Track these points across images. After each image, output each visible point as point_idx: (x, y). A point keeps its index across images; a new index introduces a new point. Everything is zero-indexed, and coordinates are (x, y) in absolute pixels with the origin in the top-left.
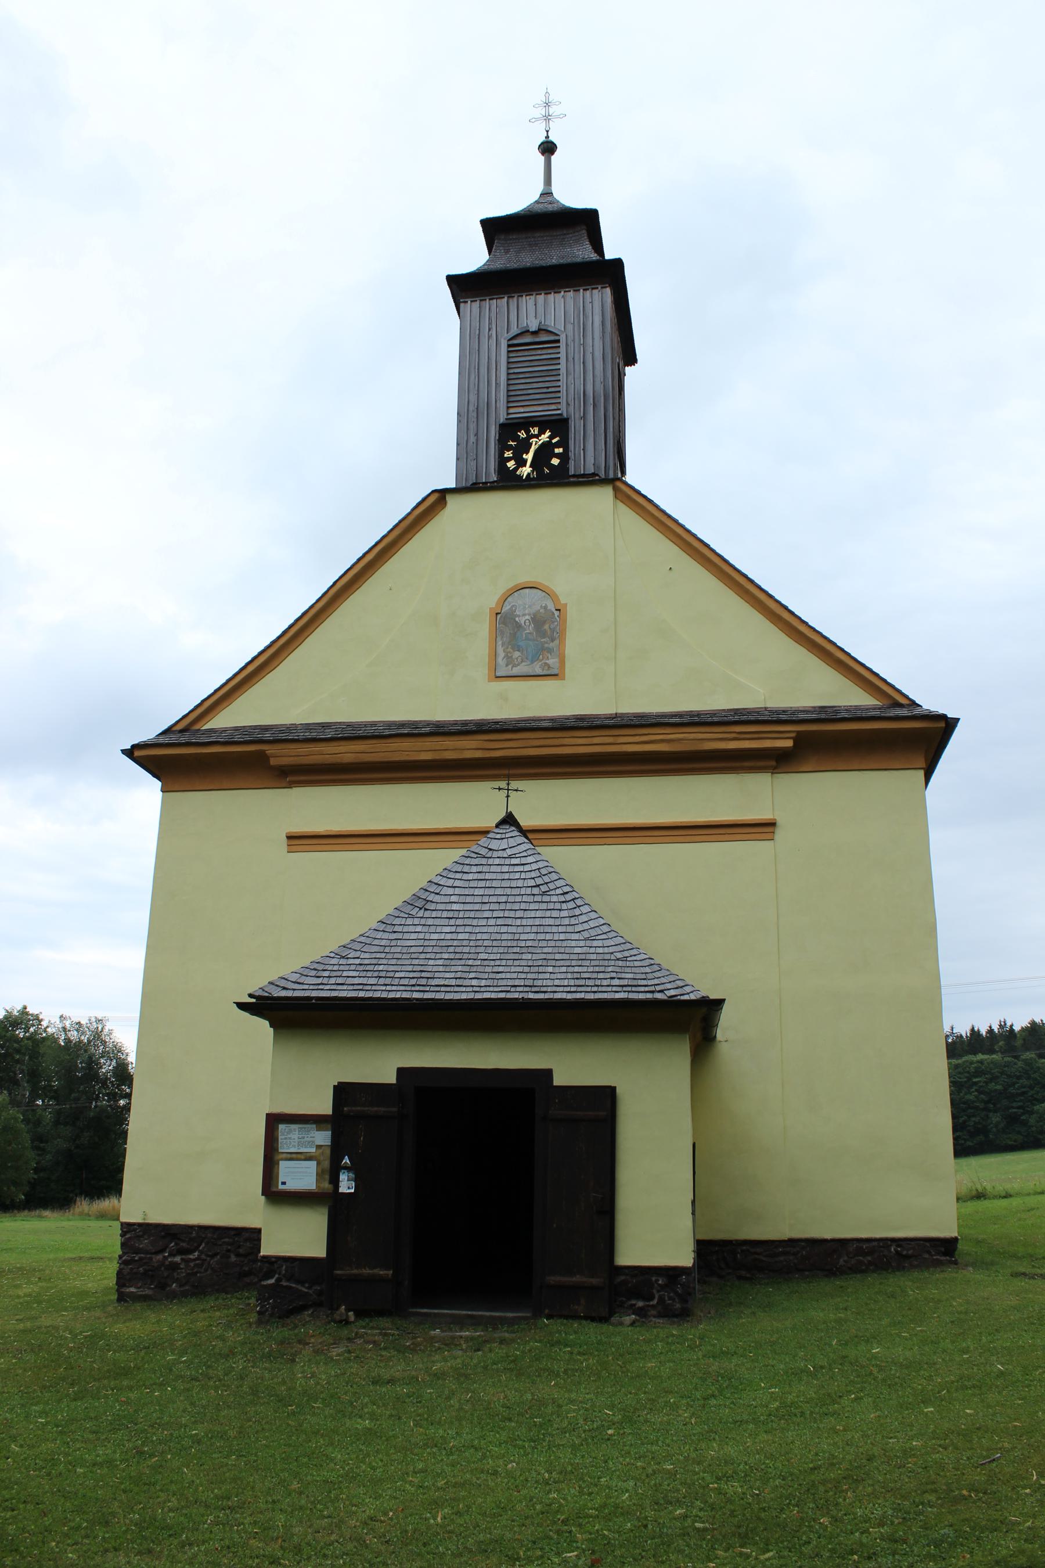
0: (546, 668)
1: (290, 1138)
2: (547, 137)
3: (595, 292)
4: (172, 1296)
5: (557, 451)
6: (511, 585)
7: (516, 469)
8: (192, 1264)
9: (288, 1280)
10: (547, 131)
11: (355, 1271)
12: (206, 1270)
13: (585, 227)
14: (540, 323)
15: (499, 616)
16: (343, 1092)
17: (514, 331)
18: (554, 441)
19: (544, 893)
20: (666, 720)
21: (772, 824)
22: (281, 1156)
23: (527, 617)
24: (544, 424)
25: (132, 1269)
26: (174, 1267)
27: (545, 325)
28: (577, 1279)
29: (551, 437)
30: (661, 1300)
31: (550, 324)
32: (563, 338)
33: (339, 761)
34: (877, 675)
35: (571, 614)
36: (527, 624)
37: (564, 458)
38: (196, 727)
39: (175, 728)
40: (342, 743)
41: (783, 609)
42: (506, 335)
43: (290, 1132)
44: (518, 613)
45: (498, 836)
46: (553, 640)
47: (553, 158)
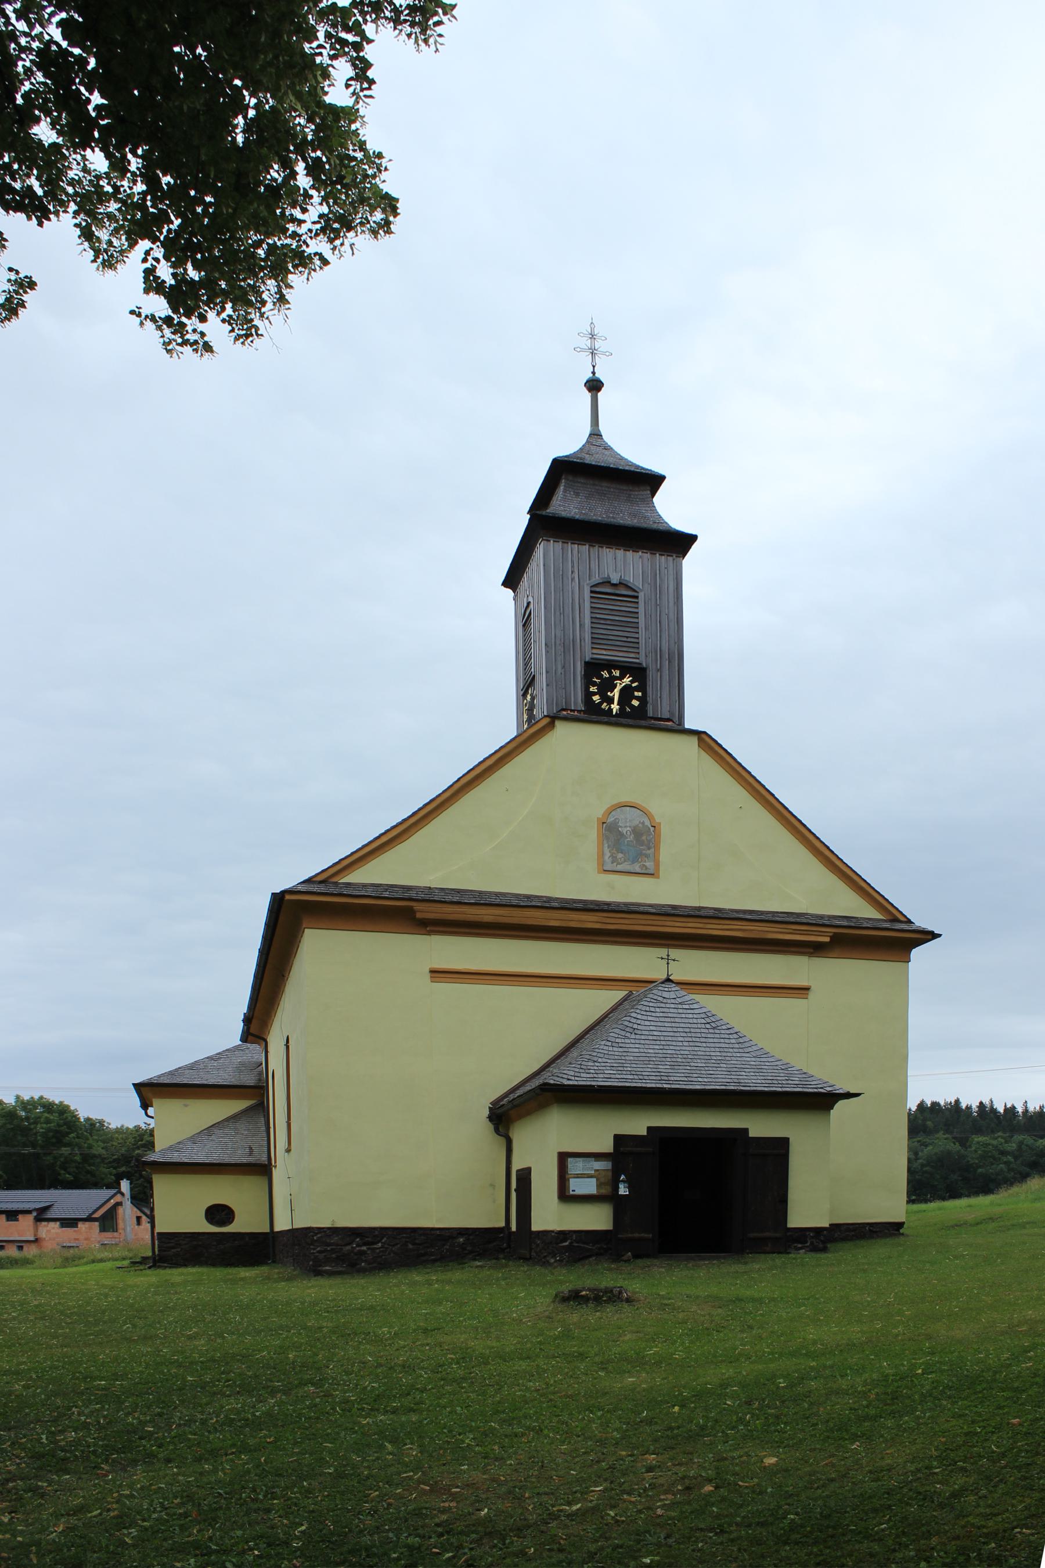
0: (644, 868)
1: (575, 1166)
2: (594, 373)
3: (670, 559)
4: (363, 1271)
5: (636, 694)
6: (615, 802)
7: (601, 703)
8: (378, 1251)
9: (577, 1243)
10: (594, 367)
11: (630, 1235)
12: (389, 1254)
13: (649, 488)
14: (621, 577)
15: (605, 825)
16: (618, 1139)
17: (596, 579)
18: (634, 685)
19: (714, 1028)
20: (741, 916)
21: (807, 989)
22: (570, 1176)
23: (628, 829)
24: (626, 669)
25: (325, 1256)
26: (363, 1253)
27: (624, 580)
28: (767, 1234)
29: (632, 682)
30: (812, 1243)
31: (630, 579)
32: (641, 595)
33: (480, 920)
34: (887, 900)
35: (664, 830)
36: (628, 833)
37: (643, 700)
38: (334, 880)
39: (314, 879)
40: (484, 907)
41: (826, 848)
42: (588, 582)
43: (577, 1162)
44: (620, 824)
45: (666, 989)
46: (649, 849)
47: (599, 394)
